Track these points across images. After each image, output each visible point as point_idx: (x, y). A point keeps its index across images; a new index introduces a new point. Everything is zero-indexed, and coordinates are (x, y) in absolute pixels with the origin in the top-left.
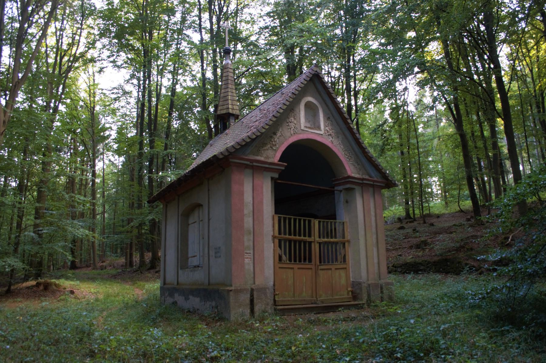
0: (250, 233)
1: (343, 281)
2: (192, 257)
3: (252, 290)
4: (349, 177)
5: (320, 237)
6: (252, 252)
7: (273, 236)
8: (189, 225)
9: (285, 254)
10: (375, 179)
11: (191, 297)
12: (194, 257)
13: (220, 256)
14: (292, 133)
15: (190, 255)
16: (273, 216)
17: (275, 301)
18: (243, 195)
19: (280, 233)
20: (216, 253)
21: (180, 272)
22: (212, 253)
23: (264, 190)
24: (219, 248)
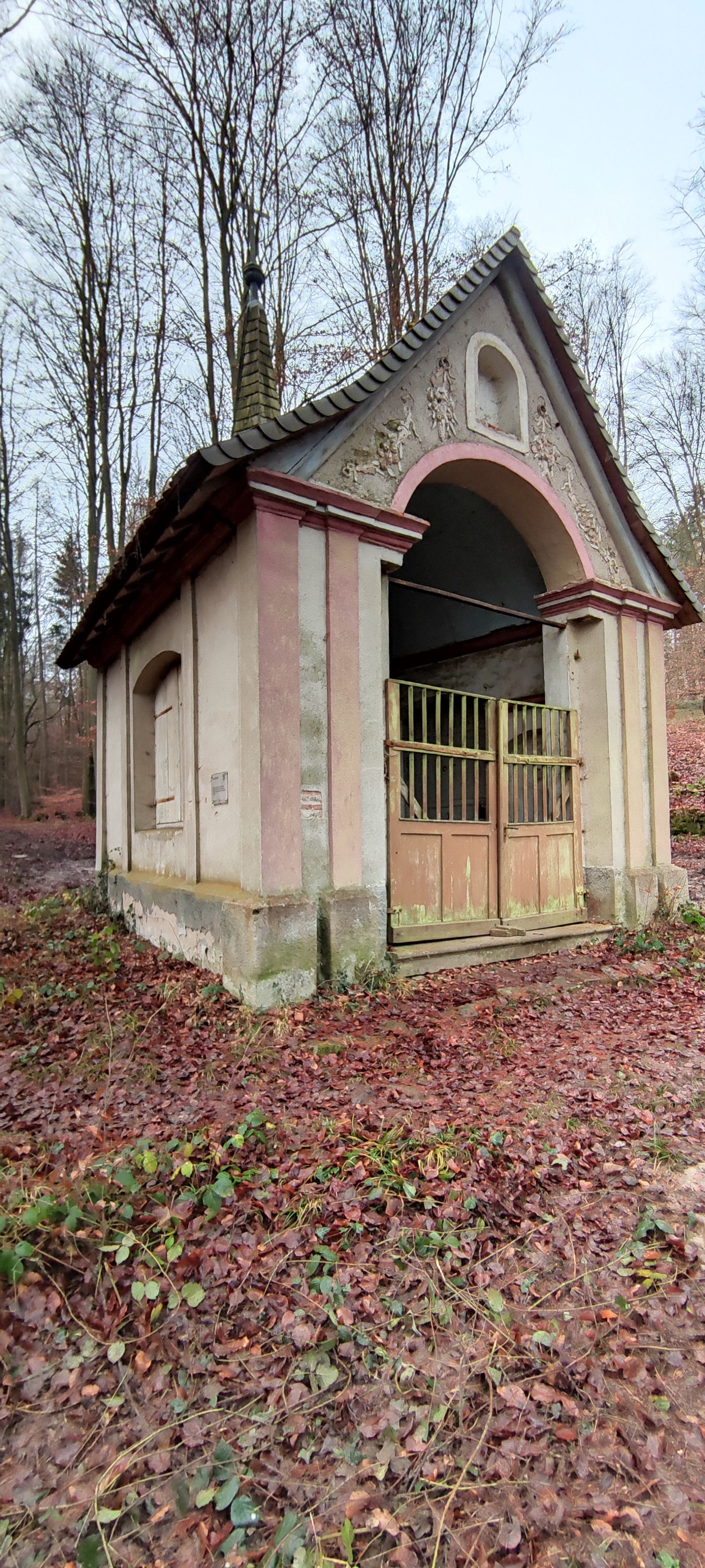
0: (318, 731)
1: (566, 870)
2: (163, 801)
3: (323, 905)
4: (591, 585)
5: (511, 750)
6: (323, 788)
7: (385, 742)
8: (155, 718)
9: (419, 796)
10: (653, 595)
11: (156, 908)
12: (168, 800)
13: (227, 802)
14: (443, 435)
15: (159, 796)
16: (386, 682)
17: (390, 931)
18: (296, 606)
19: (405, 736)
20: (215, 790)
21: (135, 837)
22: (205, 791)
23: (362, 598)
24: (225, 775)
